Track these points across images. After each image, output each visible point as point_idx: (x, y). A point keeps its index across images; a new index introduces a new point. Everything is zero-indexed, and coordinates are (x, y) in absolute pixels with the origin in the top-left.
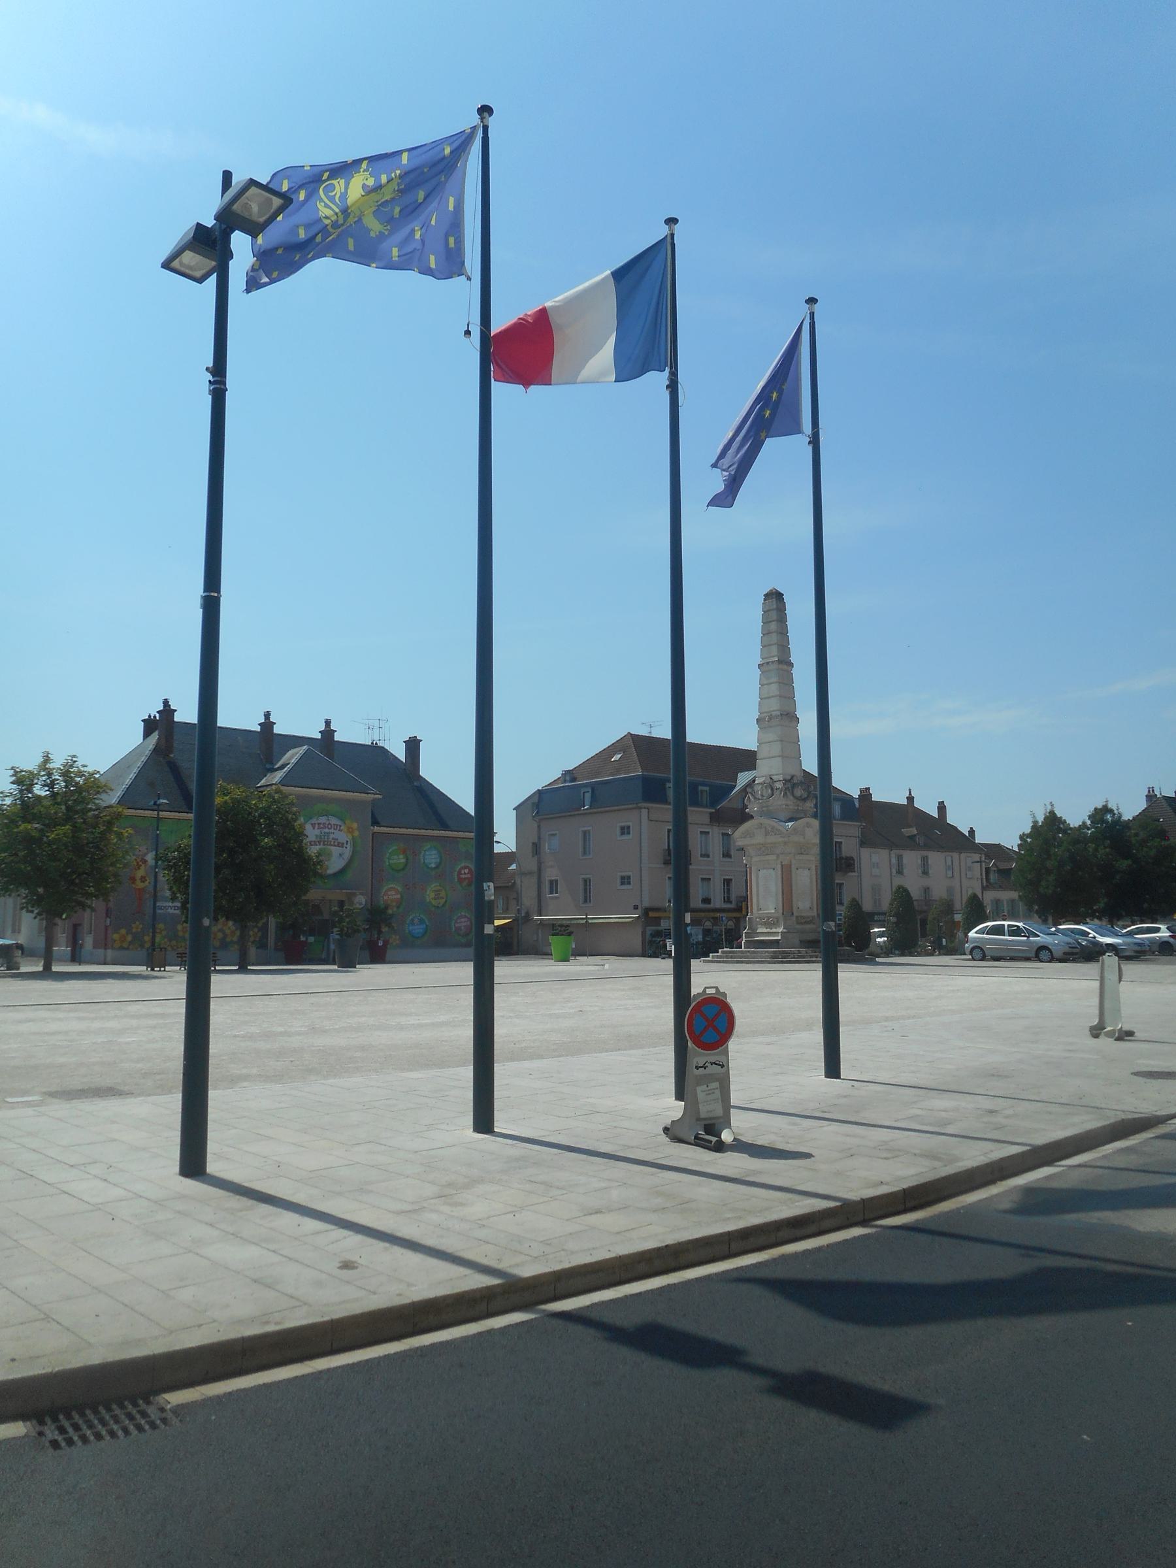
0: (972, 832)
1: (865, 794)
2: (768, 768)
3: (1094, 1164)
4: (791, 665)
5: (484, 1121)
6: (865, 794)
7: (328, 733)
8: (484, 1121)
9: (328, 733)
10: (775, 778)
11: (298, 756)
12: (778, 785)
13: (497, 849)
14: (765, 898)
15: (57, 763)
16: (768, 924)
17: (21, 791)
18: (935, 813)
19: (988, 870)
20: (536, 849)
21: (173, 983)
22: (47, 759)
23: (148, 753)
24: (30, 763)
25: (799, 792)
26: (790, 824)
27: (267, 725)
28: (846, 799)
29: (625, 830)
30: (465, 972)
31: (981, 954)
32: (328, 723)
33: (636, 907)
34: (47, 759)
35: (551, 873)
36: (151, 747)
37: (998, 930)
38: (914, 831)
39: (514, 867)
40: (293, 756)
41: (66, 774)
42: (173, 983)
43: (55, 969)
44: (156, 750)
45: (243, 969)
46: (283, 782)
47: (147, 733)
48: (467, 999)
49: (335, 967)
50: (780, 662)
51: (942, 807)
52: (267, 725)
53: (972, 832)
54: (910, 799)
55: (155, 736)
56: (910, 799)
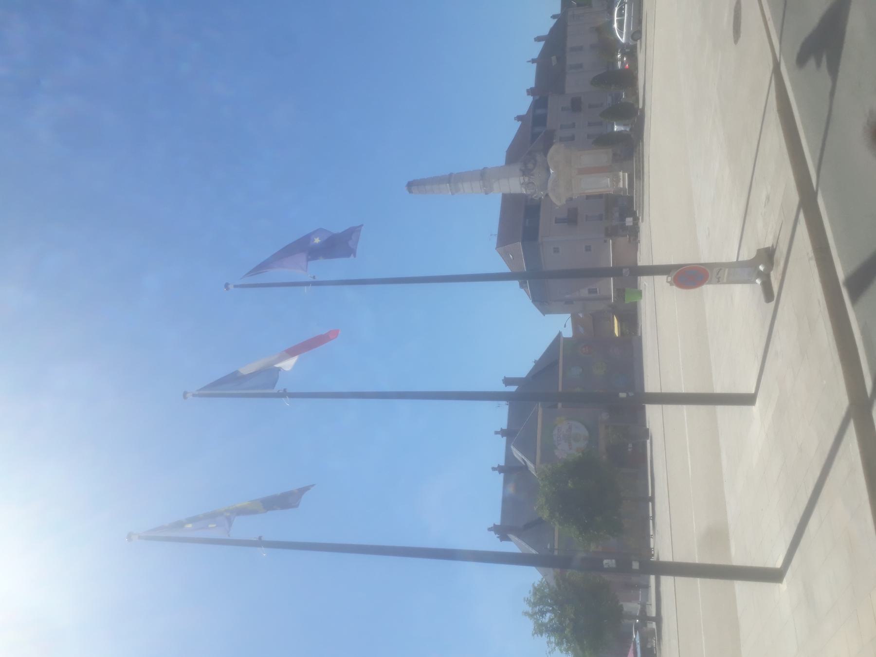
0: (554, 17)
1: (531, 92)
2: (515, 185)
3: (818, 155)
4: (451, 175)
5: (747, 400)
6: (531, 92)
7: (503, 433)
8: (747, 400)
9: (503, 433)
10: (522, 181)
11: (517, 452)
12: (527, 179)
13: (568, 333)
14: (603, 184)
15: (529, 609)
16: (618, 181)
17: (546, 631)
18: (541, 44)
19: (579, 5)
20: (569, 302)
21: (653, 414)
22: (526, 613)
23: (520, 541)
24: (530, 624)
25: (530, 166)
26: (552, 171)
27: (500, 469)
28: (535, 105)
29: (556, 250)
30: (667, 581)
31: (636, 34)
32: (496, 433)
33: (605, 241)
34: (526, 613)
35: (584, 293)
36: (517, 539)
37: (621, 23)
38: (554, 58)
39: (581, 315)
40: (518, 455)
41: (534, 605)
42: (645, 282)
43: (654, 614)
44: (519, 536)
45: (652, 499)
46: (534, 463)
47: (509, 539)
48: (670, 409)
49: (648, 441)
50: (449, 182)
51: (538, 39)
52: (500, 469)
53: (554, 17)
54: (533, 61)
55: (511, 536)
56: (533, 61)
